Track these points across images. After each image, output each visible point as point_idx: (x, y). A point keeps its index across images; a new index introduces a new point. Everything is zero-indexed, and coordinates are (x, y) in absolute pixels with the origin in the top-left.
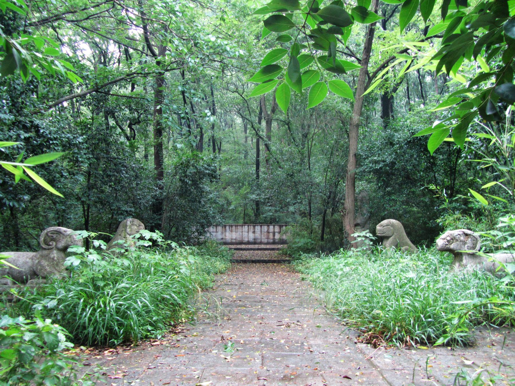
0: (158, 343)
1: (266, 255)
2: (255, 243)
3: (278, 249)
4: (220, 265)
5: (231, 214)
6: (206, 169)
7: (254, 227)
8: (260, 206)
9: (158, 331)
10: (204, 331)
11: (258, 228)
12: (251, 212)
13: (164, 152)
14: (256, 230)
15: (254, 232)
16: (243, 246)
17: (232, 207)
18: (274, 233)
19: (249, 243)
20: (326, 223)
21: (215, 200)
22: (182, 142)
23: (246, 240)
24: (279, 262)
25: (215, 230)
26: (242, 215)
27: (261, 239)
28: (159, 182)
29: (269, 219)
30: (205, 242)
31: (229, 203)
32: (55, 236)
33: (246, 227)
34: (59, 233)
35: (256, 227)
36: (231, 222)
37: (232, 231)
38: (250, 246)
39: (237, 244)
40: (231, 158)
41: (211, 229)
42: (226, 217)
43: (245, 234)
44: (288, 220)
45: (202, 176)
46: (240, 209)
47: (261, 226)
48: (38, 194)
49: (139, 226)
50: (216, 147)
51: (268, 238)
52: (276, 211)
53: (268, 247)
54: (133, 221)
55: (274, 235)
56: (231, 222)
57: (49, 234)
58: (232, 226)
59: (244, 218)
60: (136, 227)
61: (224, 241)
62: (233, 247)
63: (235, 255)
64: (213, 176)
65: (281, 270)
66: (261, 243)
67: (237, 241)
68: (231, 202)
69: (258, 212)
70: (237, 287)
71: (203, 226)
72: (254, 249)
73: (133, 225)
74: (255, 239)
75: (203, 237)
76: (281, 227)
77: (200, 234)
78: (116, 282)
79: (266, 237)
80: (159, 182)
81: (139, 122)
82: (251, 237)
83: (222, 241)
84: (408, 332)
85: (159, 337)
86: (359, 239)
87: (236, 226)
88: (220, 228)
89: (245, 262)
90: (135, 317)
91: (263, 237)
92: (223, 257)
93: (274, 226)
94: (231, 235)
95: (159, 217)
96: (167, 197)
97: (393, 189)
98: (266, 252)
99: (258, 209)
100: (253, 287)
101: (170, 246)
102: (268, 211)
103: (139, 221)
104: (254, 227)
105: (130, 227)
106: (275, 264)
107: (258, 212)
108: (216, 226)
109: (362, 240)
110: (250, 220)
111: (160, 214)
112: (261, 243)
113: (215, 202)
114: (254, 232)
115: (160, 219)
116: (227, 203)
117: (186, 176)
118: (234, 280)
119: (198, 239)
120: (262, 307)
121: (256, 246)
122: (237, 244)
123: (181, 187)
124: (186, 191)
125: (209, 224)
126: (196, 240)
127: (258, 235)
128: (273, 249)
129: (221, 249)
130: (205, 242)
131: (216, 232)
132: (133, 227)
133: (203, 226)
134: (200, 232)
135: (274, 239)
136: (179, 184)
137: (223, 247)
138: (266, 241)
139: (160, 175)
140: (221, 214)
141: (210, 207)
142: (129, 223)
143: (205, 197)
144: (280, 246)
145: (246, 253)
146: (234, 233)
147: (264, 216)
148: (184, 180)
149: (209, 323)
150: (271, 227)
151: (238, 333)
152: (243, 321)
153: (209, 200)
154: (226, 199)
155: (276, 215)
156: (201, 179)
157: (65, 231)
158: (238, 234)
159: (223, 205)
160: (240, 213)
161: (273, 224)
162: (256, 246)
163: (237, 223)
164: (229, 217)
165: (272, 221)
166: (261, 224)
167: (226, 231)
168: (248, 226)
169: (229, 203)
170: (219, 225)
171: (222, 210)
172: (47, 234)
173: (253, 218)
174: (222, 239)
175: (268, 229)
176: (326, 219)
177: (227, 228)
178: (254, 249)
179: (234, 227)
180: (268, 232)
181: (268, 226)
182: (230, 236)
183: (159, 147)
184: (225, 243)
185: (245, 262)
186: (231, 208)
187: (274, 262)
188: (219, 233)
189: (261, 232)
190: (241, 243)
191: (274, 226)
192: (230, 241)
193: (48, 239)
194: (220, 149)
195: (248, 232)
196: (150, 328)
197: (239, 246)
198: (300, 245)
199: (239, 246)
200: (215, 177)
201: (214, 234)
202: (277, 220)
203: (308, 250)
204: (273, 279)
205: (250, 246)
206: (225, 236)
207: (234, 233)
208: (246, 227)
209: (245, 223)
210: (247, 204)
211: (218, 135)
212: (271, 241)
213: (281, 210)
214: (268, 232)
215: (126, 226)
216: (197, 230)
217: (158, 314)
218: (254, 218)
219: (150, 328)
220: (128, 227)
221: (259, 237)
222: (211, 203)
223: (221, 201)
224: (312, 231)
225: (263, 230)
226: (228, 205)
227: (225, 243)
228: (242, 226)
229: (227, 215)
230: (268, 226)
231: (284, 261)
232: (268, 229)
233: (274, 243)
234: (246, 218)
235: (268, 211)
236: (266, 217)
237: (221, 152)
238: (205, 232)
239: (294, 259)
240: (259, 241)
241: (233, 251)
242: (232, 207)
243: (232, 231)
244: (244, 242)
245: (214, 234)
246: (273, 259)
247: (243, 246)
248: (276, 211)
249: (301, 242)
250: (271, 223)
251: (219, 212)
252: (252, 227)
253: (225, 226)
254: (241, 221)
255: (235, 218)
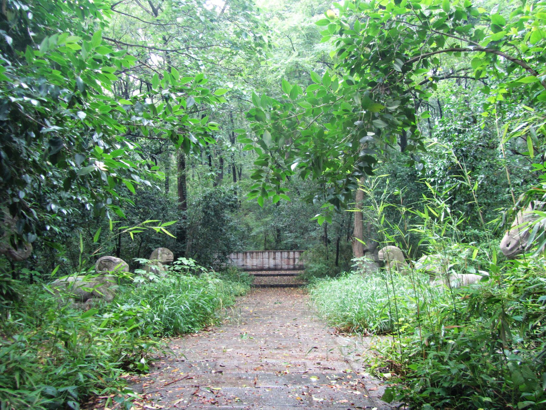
0: (196, 335)
1: (284, 280)
2: (275, 269)
3: (297, 275)
4: (240, 288)
5: (252, 241)
6: (229, 201)
7: (275, 253)
8: (281, 232)
9: (196, 328)
10: (227, 330)
11: (278, 255)
12: (271, 238)
13: (188, 184)
14: (277, 256)
15: (274, 259)
16: (264, 272)
17: (253, 233)
18: (294, 260)
19: (269, 269)
20: (340, 249)
21: (235, 227)
22: (165, 7)
23: (267, 266)
24: (296, 286)
25: (236, 257)
26: (263, 241)
27: (282, 265)
28: (183, 213)
29: (289, 245)
30: (227, 268)
31: (250, 229)
32: (107, 264)
33: (267, 253)
34: (110, 261)
35: (277, 253)
36: (252, 248)
37: (252, 258)
38: (270, 272)
39: (258, 270)
40: (252, 184)
41: (233, 256)
42: (247, 244)
43: (266, 260)
44: (309, 246)
45: (223, 207)
46: (261, 235)
47: (281, 252)
48: (150, 246)
49: (169, 254)
50: (237, 172)
51: (288, 264)
52: (296, 237)
53: (288, 272)
54: (163, 250)
55: (294, 261)
56: (252, 248)
57: (103, 262)
58: (252, 253)
59: (265, 244)
60: (166, 255)
61: (245, 267)
62: (254, 273)
63: (255, 281)
64: (234, 207)
65: (296, 293)
66: (281, 269)
67: (258, 268)
68: (253, 229)
69: (279, 239)
70: (254, 305)
71: (224, 254)
72: (274, 275)
73: (163, 253)
74: (275, 265)
75: (225, 264)
76: (301, 252)
77: (222, 261)
78: (166, 294)
79: (286, 263)
80: (183, 213)
81: (161, 152)
82: (272, 263)
83: (243, 267)
84: (366, 326)
85: (197, 332)
86: (358, 263)
87: (256, 252)
88: (240, 255)
89: (264, 286)
90: (181, 317)
91: (283, 264)
92: (243, 282)
93: (294, 252)
94: (252, 262)
95: (183, 245)
96: (190, 227)
97: (56, 311)
98: (285, 278)
99: (278, 236)
100: (267, 305)
101: (200, 270)
102: (289, 238)
103: (168, 250)
104: (275, 253)
105: (161, 255)
106: (292, 288)
107: (279, 239)
108: (237, 253)
109: (360, 264)
110: (271, 246)
111: (184, 243)
112: (281, 269)
113: (235, 229)
114: (274, 259)
115: (184, 247)
116: (248, 229)
117: (208, 207)
118: (252, 300)
119: (220, 266)
120: (272, 317)
121: (277, 272)
122: (258, 270)
123: (204, 217)
124: (209, 220)
125: (231, 252)
126: (218, 267)
127: (278, 261)
128: (292, 275)
129: (241, 275)
130: (227, 268)
131: (237, 259)
132: (163, 255)
133: (224, 254)
134: (222, 259)
135: (294, 265)
136: (202, 215)
137: (244, 273)
138: (286, 267)
139: (184, 206)
140: (242, 241)
141: (231, 234)
142: (160, 251)
143: (226, 225)
144: (299, 272)
145: (266, 278)
146: (255, 260)
147: (285, 242)
148: (207, 212)
149: (231, 326)
150: (291, 253)
151: (252, 330)
152: (256, 325)
153: (230, 228)
154: (247, 225)
155: (297, 241)
156: (222, 209)
157: (115, 260)
158: (258, 260)
159: (244, 232)
160: (261, 240)
161: (294, 250)
162: (277, 272)
163: (259, 249)
164: (251, 244)
165: (293, 247)
166: (282, 250)
167: (246, 258)
168: (269, 252)
169: (250, 229)
170: (240, 252)
171: (243, 237)
172: (101, 262)
173: (274, 244)
174: (243, 265)
175: (289, 255)
176: (340, 245)
177: (248, 254)
178: (274, 275)
179: (255, 254)
180: (288, 258)
181: (289, 252)
182: (251, 262)
183: (182, 180)
184: (246, 270)
185: (264, 286)
186: (252, 234)
187: (291, 286)
188: (240, 260)
189: (281, 258)
190: (262, 269)
191: (294, 252)
192: (251, 268)
193: (102, 267)
194: (240, 174)
195: (269, 258)
196: (190, 326)
197: (260, 273)
198: (314, 270)
199: (260, 273)
200: (236, 207)
201: (235, 261)
202: (299, 245)
203: (321, 275)
204: (287, 299)
205: (270, 272)
206: (246, 262)
207: (255, 260)
208: (267, 253)
209: (266, 249)
210: (267, 230)
211: (238, 162)
212: (292, 267)
213: (302, 236)
214: (288, 258)
215: (158, 254)
216: (219, 257)
217: (195, 317)
218: (275, 244)
219: (190, 326)
220: (159, 256)
221: (280, 264)
222: (232, 230)
223: (243, 228)
224: (328, 256)
225: (283, 256)
226: (248, 232)
227: (246, 270)
228: (263, 252)
229: (247, 242)
230: (289, 252)
231: (301, 285)
232: (289, 255)
233: (294, 269)
234: (267, 245)
235: (289, 238)
236: (286, 244)
237: (242, 176)
238: (226, 259)
239: (309, 283)
240: (279, 267)
241: (253, 277)
242: (253, 233)
243: (252, 258)
244: (265, 268)
245: (235, 261)
246: (291, 283)
247: (264, 272)
248: (296, 237)
249: (316, 267)
250: (292, 249)
251: (239, 238)
252: (272, 253)
253: (246, 253)
254: (262, 248)
255: (256, 244)
